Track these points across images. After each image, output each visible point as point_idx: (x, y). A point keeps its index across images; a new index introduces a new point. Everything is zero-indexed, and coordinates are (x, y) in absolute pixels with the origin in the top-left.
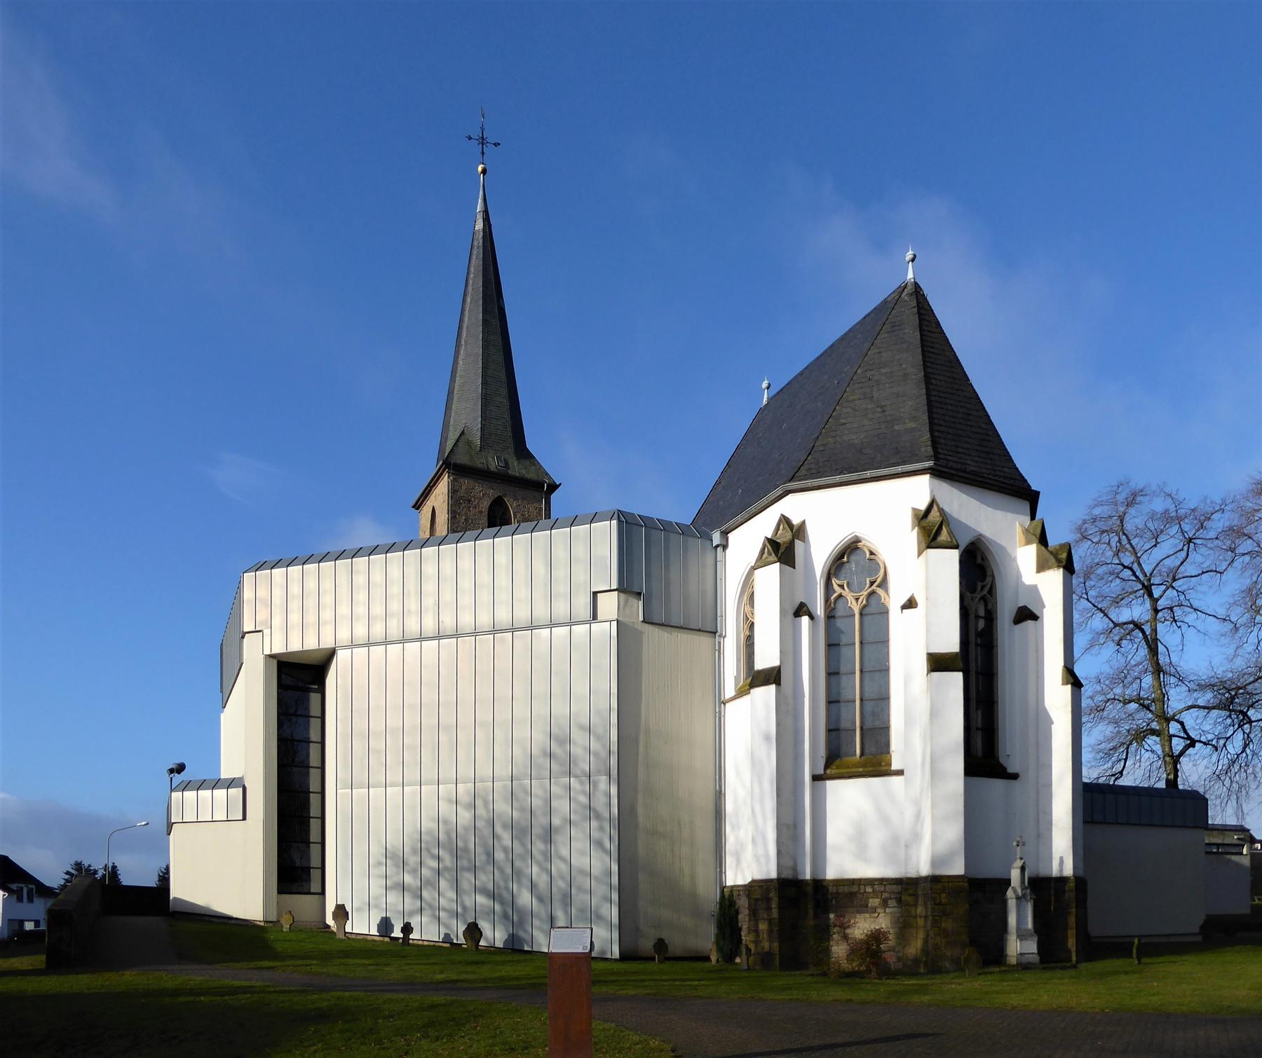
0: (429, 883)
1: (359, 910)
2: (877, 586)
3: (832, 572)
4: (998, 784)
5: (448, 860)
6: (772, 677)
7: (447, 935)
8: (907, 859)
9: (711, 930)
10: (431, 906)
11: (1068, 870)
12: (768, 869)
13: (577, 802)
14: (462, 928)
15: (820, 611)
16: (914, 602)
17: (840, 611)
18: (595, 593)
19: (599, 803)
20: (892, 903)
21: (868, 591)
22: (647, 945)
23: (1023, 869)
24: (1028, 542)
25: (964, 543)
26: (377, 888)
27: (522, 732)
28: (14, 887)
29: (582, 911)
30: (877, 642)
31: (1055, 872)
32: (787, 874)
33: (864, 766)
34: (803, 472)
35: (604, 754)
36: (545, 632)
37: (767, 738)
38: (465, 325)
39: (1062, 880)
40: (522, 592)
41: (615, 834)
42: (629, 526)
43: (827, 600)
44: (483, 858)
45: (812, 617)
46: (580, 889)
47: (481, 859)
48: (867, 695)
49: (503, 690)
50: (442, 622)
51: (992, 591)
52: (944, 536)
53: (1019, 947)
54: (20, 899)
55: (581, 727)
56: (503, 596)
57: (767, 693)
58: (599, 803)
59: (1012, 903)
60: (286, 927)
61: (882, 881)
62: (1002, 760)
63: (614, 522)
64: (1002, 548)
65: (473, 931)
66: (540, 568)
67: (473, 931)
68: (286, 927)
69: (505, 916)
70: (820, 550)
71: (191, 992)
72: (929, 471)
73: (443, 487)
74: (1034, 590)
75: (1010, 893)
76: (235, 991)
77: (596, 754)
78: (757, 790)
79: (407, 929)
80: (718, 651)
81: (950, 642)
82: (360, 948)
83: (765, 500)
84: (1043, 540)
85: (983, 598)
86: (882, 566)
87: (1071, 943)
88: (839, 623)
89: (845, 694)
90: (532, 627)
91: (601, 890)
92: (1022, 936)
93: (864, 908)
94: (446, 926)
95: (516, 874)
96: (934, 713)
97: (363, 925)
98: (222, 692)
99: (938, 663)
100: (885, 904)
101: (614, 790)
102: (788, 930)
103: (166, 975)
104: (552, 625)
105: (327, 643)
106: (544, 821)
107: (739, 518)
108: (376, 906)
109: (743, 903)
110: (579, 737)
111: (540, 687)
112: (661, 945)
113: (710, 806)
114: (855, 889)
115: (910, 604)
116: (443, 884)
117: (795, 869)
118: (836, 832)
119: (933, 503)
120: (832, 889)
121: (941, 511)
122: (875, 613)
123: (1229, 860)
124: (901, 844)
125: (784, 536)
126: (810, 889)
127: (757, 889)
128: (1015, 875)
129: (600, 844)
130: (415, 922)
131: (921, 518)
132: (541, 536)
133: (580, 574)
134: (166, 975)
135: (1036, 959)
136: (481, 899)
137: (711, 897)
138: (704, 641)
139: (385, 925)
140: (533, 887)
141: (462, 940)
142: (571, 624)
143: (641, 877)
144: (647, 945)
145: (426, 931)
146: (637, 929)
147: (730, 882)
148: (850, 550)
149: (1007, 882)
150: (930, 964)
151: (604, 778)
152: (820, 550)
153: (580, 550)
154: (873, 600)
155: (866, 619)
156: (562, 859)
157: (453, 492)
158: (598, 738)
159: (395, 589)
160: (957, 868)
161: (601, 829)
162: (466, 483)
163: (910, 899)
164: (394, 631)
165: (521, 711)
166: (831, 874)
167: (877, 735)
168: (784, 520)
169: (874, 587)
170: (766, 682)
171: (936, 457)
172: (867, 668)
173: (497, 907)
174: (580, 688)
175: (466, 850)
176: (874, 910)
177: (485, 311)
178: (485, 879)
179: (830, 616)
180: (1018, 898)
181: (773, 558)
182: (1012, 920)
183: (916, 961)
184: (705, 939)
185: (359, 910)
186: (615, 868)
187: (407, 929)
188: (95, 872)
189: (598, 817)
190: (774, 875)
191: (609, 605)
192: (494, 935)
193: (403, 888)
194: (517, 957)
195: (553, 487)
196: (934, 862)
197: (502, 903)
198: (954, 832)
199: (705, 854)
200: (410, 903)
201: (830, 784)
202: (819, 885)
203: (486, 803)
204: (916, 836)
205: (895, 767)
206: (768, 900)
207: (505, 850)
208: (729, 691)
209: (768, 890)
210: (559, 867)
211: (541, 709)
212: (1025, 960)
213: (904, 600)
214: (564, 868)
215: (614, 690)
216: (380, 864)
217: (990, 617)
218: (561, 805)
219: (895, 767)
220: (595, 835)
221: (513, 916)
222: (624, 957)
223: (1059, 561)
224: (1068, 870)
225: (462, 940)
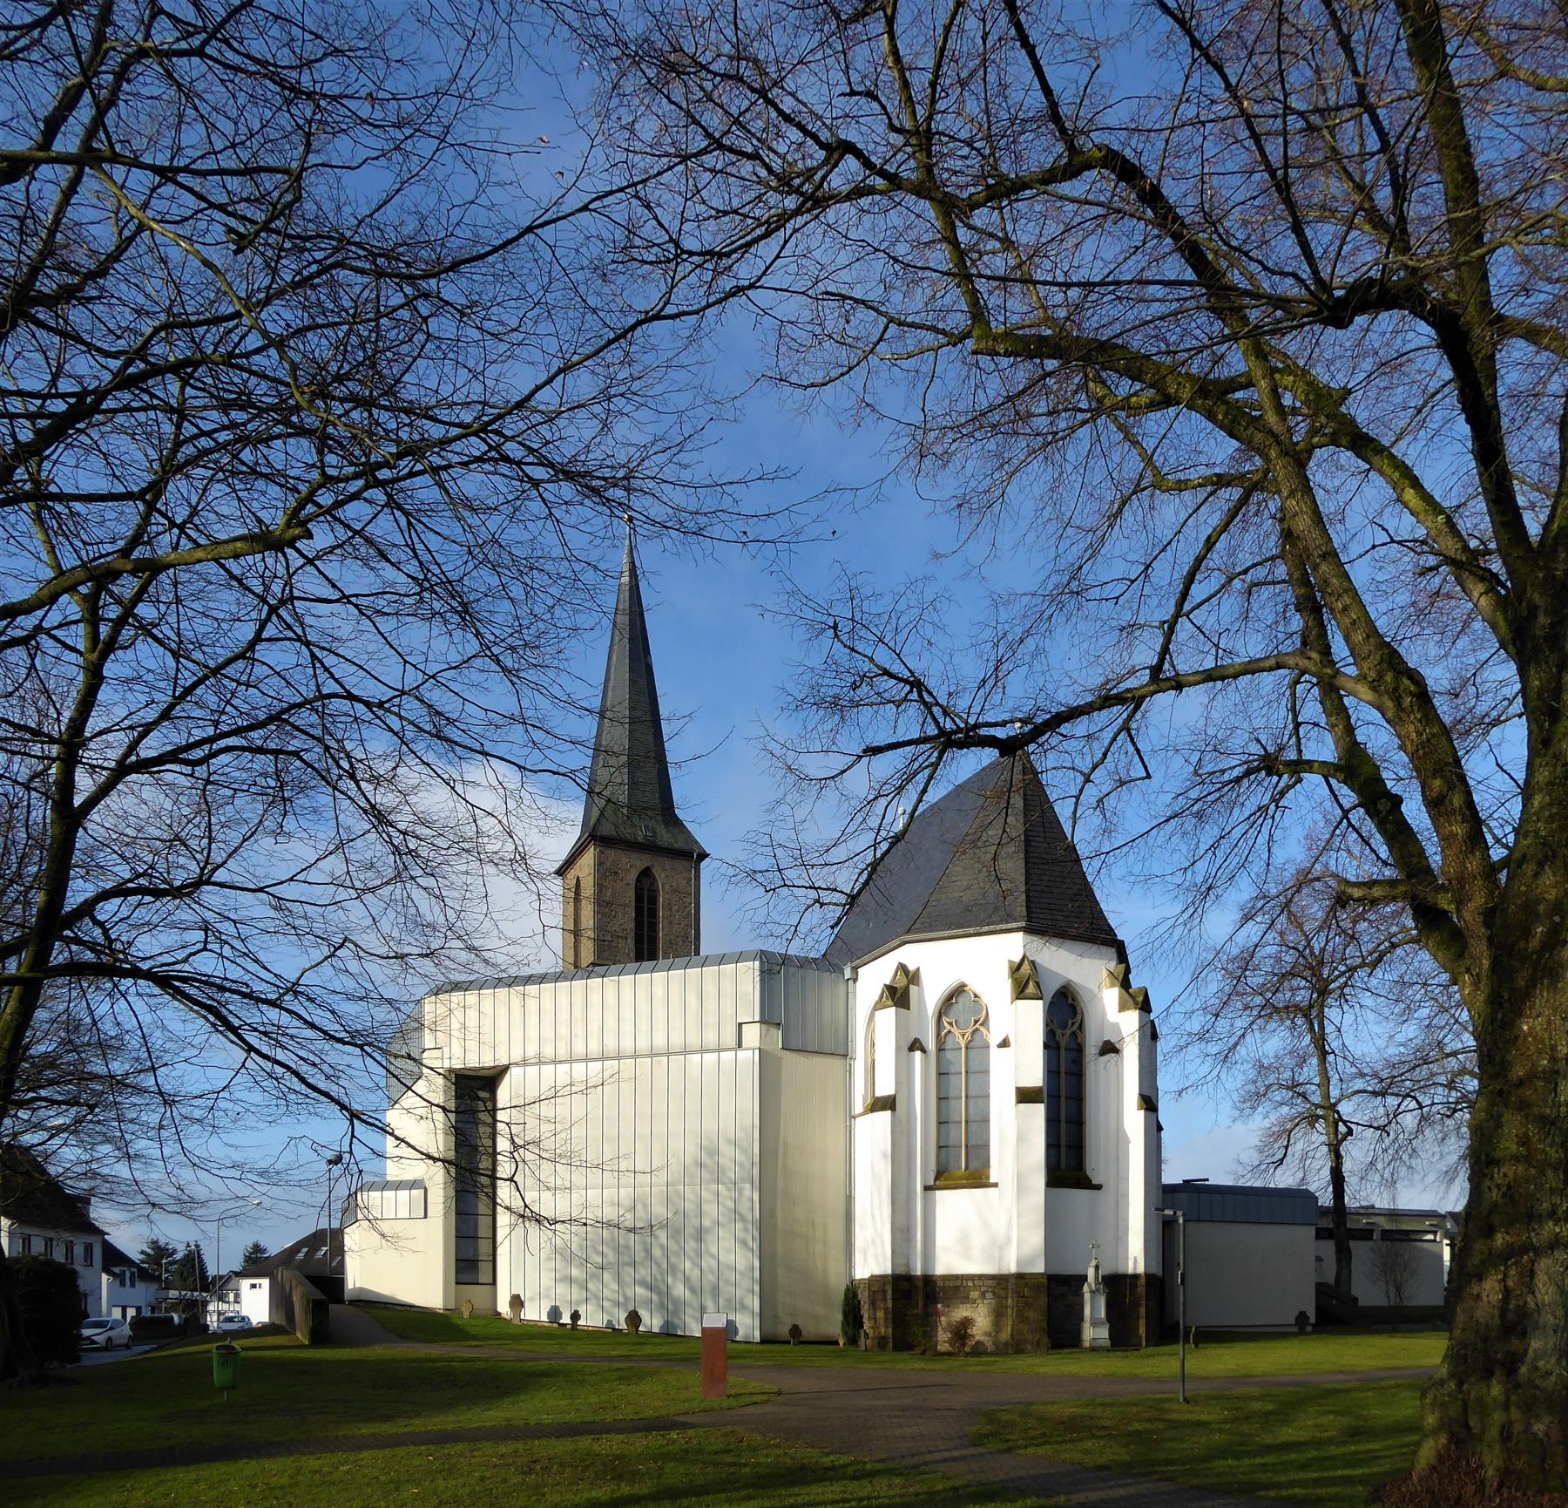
0: (594, 1275)
1: (531, 1299)
4: (1082, 1195)
5: (611, 1256)
6: (887, 1104)
7: (610, 1322)
8: (1001, 1259)
9: (839, 1317)
10: (596, 1297)
11: (1141, 1269)
12: (886, 1268)
13: (724, 1206)
14: (623, 1316)
15: (931, 1045)
17: (949, 1045)
18: (740, 1025)
19: (744, 1207)
20: (989, 1295)
22: (784, 1331)
23: (1097, 1267)
24: (1112, 985)
25: (1051, 989)
26: (547, 1279)
27: (676, 1145)
28: (117, 1270)
29: (728, 1301)
30: (979, 1073)
31: (1130, 1271)
32: (901, 1271)
33: (967, 1178)
34: (917, 925)
35: (748, 1165)
37: (885, 1155)
38: (611, 685)
39: (1136, 1277)
40: (677, 1022)
41: (756, 1234)
42: (773, 968)
43: (938, 1035)
44: (643, 1254)
45: (924, 1051)
46: (727, 1282)
47: (640, 1255)
48: (972, 1117)
49: (660, 1107)
51: (1081, 1027)
52: (1031, 988)
53: (1094, 1331)
54: (123, 1284)
55: (728, 1141)
56: (660, 1025)
57: (885, 1116)
58: (744, 1207)
59: (1087, 1296)
60: (466, 1315)
61: (981, 1277)
62: (1088, 1173)
63: (757, 963)
64: (1090, 991)
65: (634, 1318)
66: (693, 1002)
67: (634, 1318)
68: (466, 1315)
69: (662, 1305)
70: (931, 994)
71: (434, 1361)
73: (589, 857)
74: (1116, 1026)
75: (1086, 1288)
76: (471, 1360)
77: (742, 1165)
78: (876, 1199)
79: (575, 1316)
80: (849, 1072)
81: (1035, 1077)
82: (532, 1332)
83: (886, 947)
84: (1125, 984)
85: (1074, 1033)
87: (1142, 1330)
88: (949, 1055)
89: (954, 1117)
90: (685, 1052)
91: (745, 1283)
92: (1094, 1324)
93: (966, 1299)
94: (609, 1313)
95: (672, 1269)
96: (1021, 1138)
97: (535, 1312)
99: (1025, 1096)
100: (983, 1295)
101: (756, 1197)
102: (899, 1319)
104: (703, 1051)
106: (696, 1222)
107: (866, 958)
108: (547, 1296)
109: (863, 1296)
110: (726, 1150)
111: (693, 1106)
112: (795, 1331)
113: (842, 1210)
114: (958, 1283)
115: (1005, 1044)
116: (607, 1276)
117: (908, 1266)
118: (945, 1237)
119: (1024, 957)
120: (940, 1284)
121: (1033, 963)
122: (977, 1046)
123: (1422, 1249)
124: (1000, 1247)
125: (901, 982)
126: (920, 1284)
127: (874, 1280)
128: (1091, 1272)
129: (744, 1243)
130: (582, 1311)
131: (1015, 969)
132: (693, 972)
133: (727, 1007)
135: (1108, 1343)
136: (640, 1291)
137: (839, 1287)
138: (837, 1063)
139: (555, 1313)
140: (686, 1280)
141: (624, 1326)
142: (719, 1050)
143: (780, 1272)
144: (784, 1331)
145: (592, 1319)
146: (776, 1316)
147: (858, 1276)
148: (959, 991)
149: (1084, 1278)
150: (1016, 1347)
151: (748, 1186)
152: (931, 994)
153: (727, 987)
154: (977, 1035)
155: (971, 1052)
156: (712, 1256)
157: (599, 864)
158: (744, 1151)
159: (563, 1015)
160: (1040, 1268)
161: (746, 1230)
162: (612, 854)
163: (1002, 1293)
164: (563, 1053)
165: (675, 1126)
166: (940, 1269)
167: (979, 1151)
168: (902, 968)
170: (883, 1108)
171: (1029, 918)
172: (971, 1093)
173: (655, 1298)
174: (727, 1108)
175: (627, 1247)
176: (974, 1301)
177: (631, 670)
178: (643, 1272)
179: (940, 1049)
180: (1091, 1292)
181: (890, 1002)
182: (1087, 1311)
183: (1006, 1344)
184: (833, 1324)
185: (531, 1299)
186: (757, 1264)
187: (575, 1316)
188: (174, 1251)
189: (743, 1219)
190: (889, 1272)
191: (752, 1034)
192: (652, 1322)
193: (571, 1280)
194: (672, 1339)
195: (703, 856)
196: (1018, 1264)
197: (659, 1293)
198: (1036, 1239)
199: (836, 1254)
200: (577, 1294)
201: (940, 1195)
202: (928, 1280)
203: (645, 1206)
204: (1008, 1239)
205: (992, 1180)
206: (885, 1292)
207: (662, 1247)
208: (859, 1107)
209: (884, 1284)
210: (708, 1263)
211: (693, 1125)
212: (1097, 1344)
213: (1000, 1040)
214: (714, 1263)
215: (757, 1122)
216: (549, 1259)
217: (1078, 1050)
218: (710, 1209)
219: (992, 1180)
220: (740, 1234)
221: (668, 1303)
222: (763, 1341)
223: (1136, 1003)
224: (1141, 1269)
225: (624, 1326)
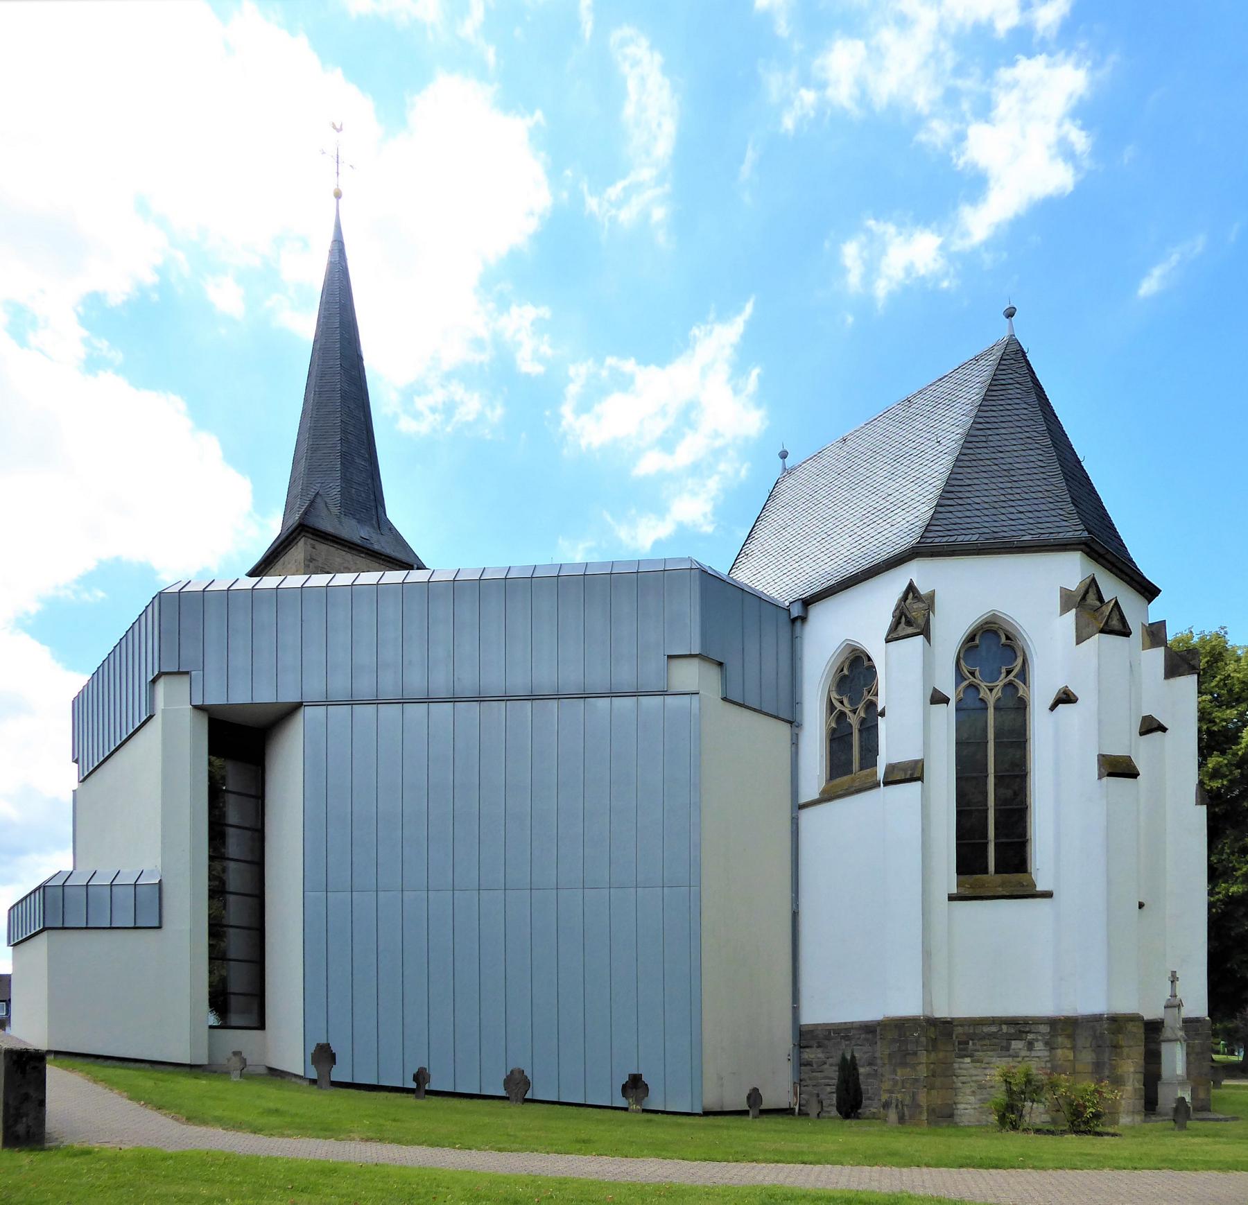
2: (1014, 677)
3: (961, 656)
16: (929, 697)
21: (1004, 681)
36: (603, 703)
50: (459, 679)
72: (1083, 547)
86: (1019, 654)
98: (420, 1086)
103: (449, 408)
105: (290, 696)
134: (449, 408)
169: (1011, 677)
205: (1040, 887)
